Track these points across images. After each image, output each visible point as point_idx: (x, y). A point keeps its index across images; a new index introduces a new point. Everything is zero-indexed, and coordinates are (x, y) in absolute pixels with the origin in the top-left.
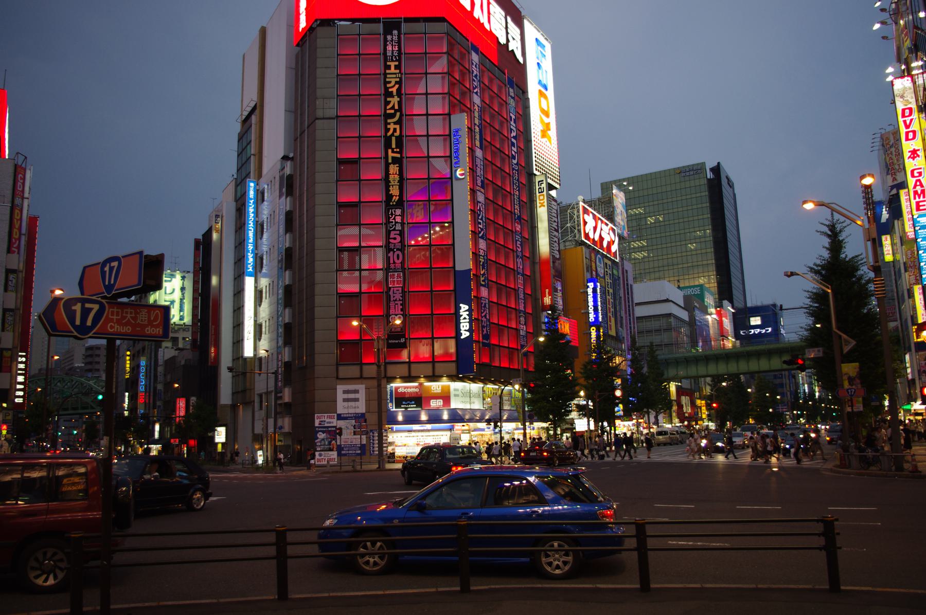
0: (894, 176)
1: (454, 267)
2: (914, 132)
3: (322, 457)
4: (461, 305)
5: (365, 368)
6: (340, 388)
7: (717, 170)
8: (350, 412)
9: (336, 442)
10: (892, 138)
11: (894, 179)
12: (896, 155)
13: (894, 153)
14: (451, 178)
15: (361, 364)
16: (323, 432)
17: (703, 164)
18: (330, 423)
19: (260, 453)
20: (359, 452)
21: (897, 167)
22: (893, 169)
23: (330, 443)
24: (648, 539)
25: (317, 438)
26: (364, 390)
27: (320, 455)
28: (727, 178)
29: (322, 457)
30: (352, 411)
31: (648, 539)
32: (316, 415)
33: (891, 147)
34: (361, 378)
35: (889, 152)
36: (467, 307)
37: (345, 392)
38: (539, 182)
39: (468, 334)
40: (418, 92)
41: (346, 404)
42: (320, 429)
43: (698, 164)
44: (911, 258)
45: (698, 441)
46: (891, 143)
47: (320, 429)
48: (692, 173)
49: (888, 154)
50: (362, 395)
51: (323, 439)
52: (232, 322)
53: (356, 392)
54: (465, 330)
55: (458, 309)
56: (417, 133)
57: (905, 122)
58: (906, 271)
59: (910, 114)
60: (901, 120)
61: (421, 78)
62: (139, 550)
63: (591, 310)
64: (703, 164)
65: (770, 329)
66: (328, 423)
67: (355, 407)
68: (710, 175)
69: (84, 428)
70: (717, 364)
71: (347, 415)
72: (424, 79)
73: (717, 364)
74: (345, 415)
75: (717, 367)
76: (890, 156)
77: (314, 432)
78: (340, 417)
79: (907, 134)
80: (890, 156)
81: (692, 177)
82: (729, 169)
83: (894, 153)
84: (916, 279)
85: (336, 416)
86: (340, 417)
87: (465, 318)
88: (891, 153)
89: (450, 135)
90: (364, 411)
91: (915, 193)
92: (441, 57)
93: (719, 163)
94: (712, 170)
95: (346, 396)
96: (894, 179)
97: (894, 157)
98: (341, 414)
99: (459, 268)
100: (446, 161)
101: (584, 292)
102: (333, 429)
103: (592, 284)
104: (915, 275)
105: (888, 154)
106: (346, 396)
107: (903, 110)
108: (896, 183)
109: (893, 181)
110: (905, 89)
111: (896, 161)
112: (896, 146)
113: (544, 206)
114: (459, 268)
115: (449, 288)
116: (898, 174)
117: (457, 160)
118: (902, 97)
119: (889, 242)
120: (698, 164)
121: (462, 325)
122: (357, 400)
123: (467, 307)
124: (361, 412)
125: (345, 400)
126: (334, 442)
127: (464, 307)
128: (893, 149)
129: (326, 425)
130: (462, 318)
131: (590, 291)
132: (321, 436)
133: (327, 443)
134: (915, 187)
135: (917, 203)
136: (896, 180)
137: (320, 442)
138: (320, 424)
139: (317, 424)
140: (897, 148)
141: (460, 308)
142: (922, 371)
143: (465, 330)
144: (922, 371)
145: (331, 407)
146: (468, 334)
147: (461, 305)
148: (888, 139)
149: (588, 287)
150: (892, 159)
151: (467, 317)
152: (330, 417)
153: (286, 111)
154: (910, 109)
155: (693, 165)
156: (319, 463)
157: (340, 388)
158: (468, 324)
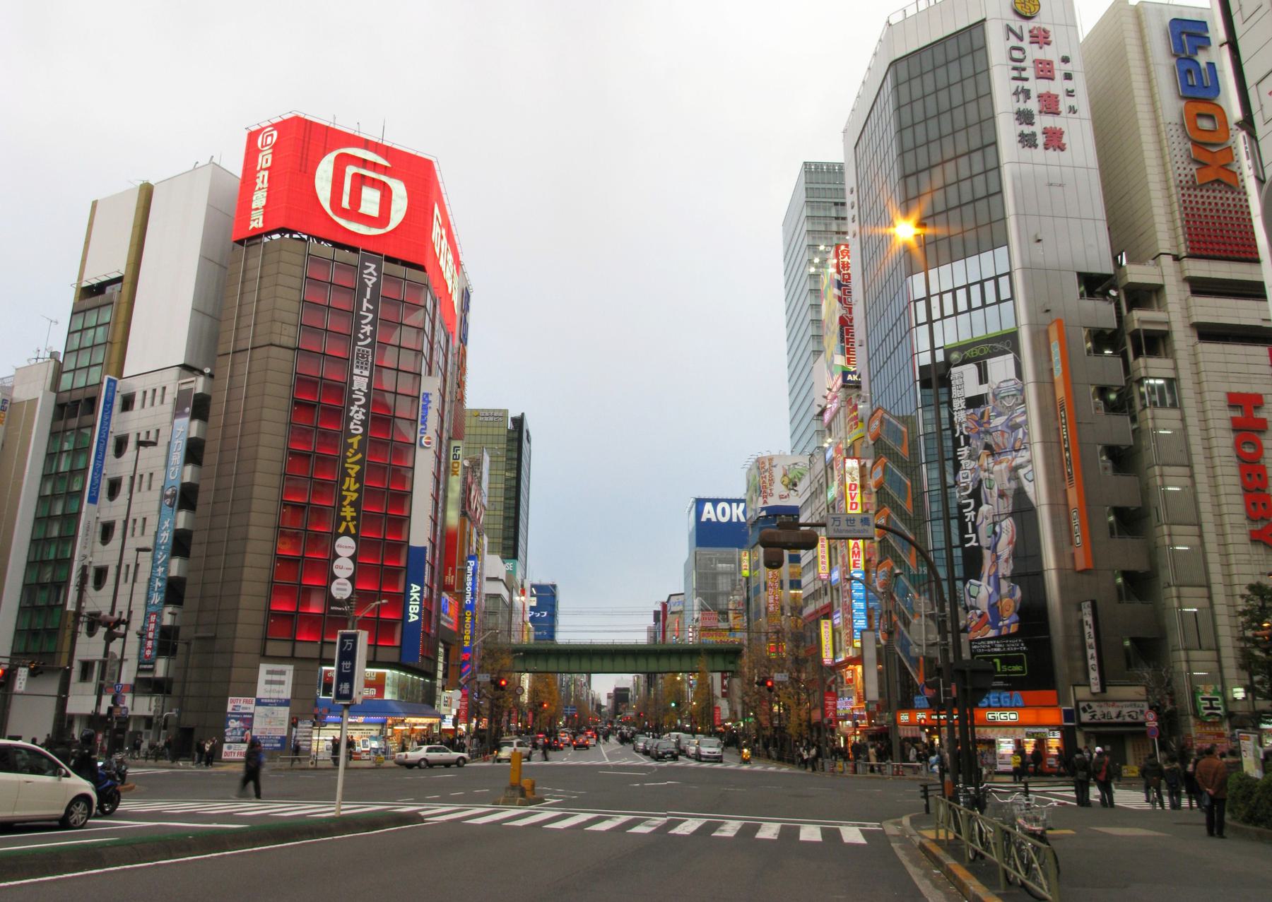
1: (408, 542)
2: (856, 504)
3: (232, 750)
4: (412, 585)
5: (298, 646)
6: (264, 668)
7: (519, 422)
8: (272, 697)
9: (251, 732)
10: (767, 464)
11: (765, 502)
14: (415, 444)
15: (294, 641)
16: (237, 719)
17: (506, 411)
18: (246, 708)
20: (279, 745)
21: (769, 491)
22: (765, 492)
23: (243, 734)
25: (228, 727)
26: (292, 672)
27: (229, 748)
28: (528, 432)
29: (232, 750)
30: (275, 695)
32: (230, 698)
34: (291, 659)
36: (419, 588)
37: (269, 672)
38: (455, 447)
39: (417, 618)
40: (391, 342)
41: (268, 687)
42: (233, 716)
43: (500, 410)
45: (988, 767)
47: (233, 716)
48: (491, 419)
50: (288, 678)
51: (235, 729)
52: (26, 555)
53: (282, 673)
54: (414, 613)
55: (408, 589)
56: (386, 388)
57: (851, 494)
58: (766, 590)
59: (855, 489)
60: (848, 492)
61: (396, 328)
64: (506, 411)
65: (546, 613)
66: (244, 708)
67: (279, 692)
68: (510, 425)
69: (1092, 765)
70: (636, 662)
71: (269, 701)
72: (399, 329)
74: (266, 701)
77: (223, 718)
78: (259, 703)
79: (852, 504)
81: (491, 424)
82: (530, 424)
85: (254, 702)
86: (259, 703)
87: (415, 600)
88: (765, 477)
89: (418, 397)
90: (289, 697)
91: (854, 552)
92: (418, 310)
93: (523, 414)
94: (514, 420)
95: (270, 677)
96: (765, 502)
97: (767, 481)
98: (260, 699)
99: (413, 543)
100: (411, 424)
102: (249, 716)
103: (473, 562)
106: (270, 677)
107: (851, 485)
108: (766, 505)
110: (853, 468)
111: (768, 486)
113: (458, 475)
114: (413, 543)
115: (399, 563)
116: (768, 497)
117: (424, 427)
118: (851, 474)
119: (747, 557)
120: (500, 410)
121: (411, 607)
122: (281, 683)
123: (419, 588)
124: (286, 698)
125: (269, 682)
126: (248, 732)
127: (415, 588)
128: (767, 474)
129: (241, 711)
130: (411, 599)
131: (470, 569)
132: (233, 724)
133: (239, 733)
134: (853, 548)
135: (854, 561)
137: (231, 731)
138: (233, 709)
139: (229, 709)
140: (770, 474)
141: (411, 588)
143: (414, 613)
145: (249, 689)
146: (417, 618)
147: (412, 585)
148: (763, 463)
149: (469, 565)
151: (418, 599)
152: (247, 702)
153: (192, 309)
154: (856, 485)
155: (494, 410)
156: (227, 757)
157: (264, 668)
158: (418, 607)
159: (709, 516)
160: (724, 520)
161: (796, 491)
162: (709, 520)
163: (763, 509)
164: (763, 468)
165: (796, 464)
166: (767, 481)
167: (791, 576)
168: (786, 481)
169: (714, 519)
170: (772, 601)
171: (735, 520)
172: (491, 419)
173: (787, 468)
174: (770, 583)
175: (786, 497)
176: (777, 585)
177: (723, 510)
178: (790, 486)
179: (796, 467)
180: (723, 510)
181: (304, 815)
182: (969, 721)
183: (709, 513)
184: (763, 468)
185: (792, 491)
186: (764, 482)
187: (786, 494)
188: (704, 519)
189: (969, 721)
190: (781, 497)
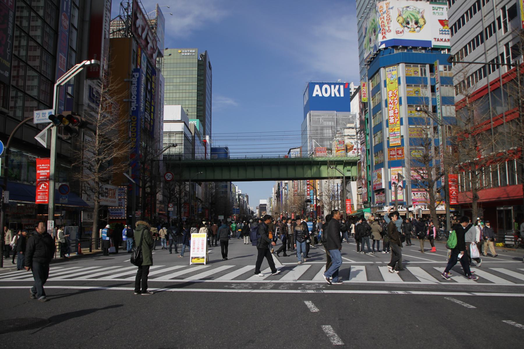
0: (384, 35)
12: (387, 19)
13: (386, 18)
19: (188, 190)
21: (387, 28)
24: (164, 124)
31: (164, 124)
33: (383, 13)
35: (382, 17)
44: (391, 97)
46: (384, 11)
49: (381, 19)
58: (386, 106)
62: (295, 148)
63: (134, 100)
70: (279, 171)
73: (287, 169)
75: (295, 170)
76: (382, 20)
80: (382, 20)
83: (386, 18)
84: (394, 113)
88: (383, 18)
96: (384, 37)
97: (385, 21)
101: (129, 81)
104: (394, 110)
105: (381, 19)
108: (385, 40)
109: (383, 38)
111: (386, 24)
112: (388, 13)
116: (387, 33)
128: (385, 15)
136: (385, 38)
142: (392, 183)
144: (392, 183)
149: (134, 76)
150: (384, 22)
159: (317, 93)
160: (327, 95)
161: (409, 28)
162: (317, 95)
163: (382, 43)
164: (382, 11)
165: (408, 7)
166: (385, 21)
167: (408, 93)
168: (401, 20)
169: (320, 95)
170: (392, 114)
171: (333, 95)
172: (188, 54)
173: (401, 10)
174: (389, 100)
175: (401, 33)
176: (397, 101)
177: (326, 89)
178: (404, 24)
179: (408, 9)
180: (326, 89)
181: (65, 268)
182: (227, 286)
183: (317, 91)
184: (382, 11)
185: (406, 28)
186: (383, 22)
187: (401, 30)
188: (314, 95)
189: (227, 286)
190: (397, 32)
